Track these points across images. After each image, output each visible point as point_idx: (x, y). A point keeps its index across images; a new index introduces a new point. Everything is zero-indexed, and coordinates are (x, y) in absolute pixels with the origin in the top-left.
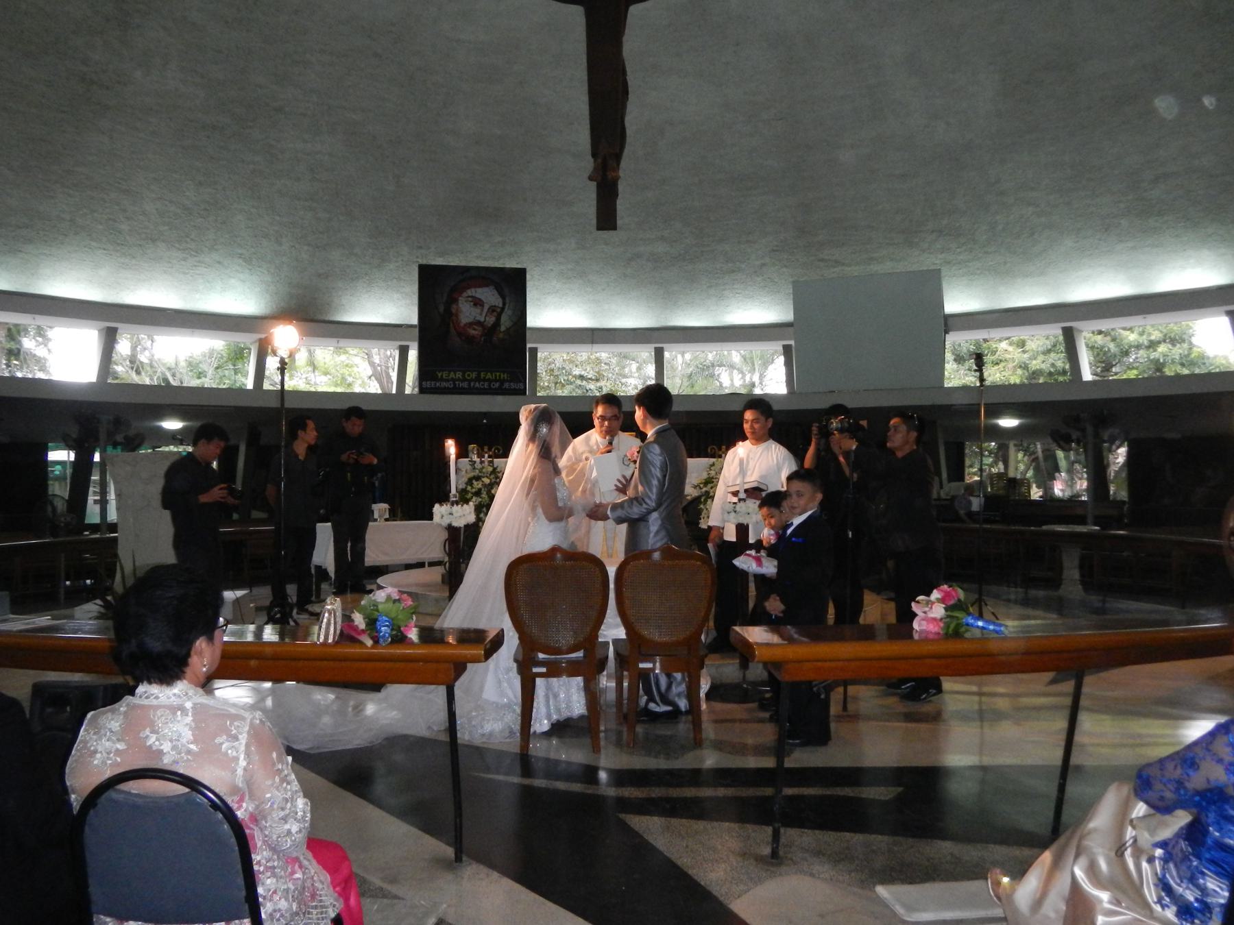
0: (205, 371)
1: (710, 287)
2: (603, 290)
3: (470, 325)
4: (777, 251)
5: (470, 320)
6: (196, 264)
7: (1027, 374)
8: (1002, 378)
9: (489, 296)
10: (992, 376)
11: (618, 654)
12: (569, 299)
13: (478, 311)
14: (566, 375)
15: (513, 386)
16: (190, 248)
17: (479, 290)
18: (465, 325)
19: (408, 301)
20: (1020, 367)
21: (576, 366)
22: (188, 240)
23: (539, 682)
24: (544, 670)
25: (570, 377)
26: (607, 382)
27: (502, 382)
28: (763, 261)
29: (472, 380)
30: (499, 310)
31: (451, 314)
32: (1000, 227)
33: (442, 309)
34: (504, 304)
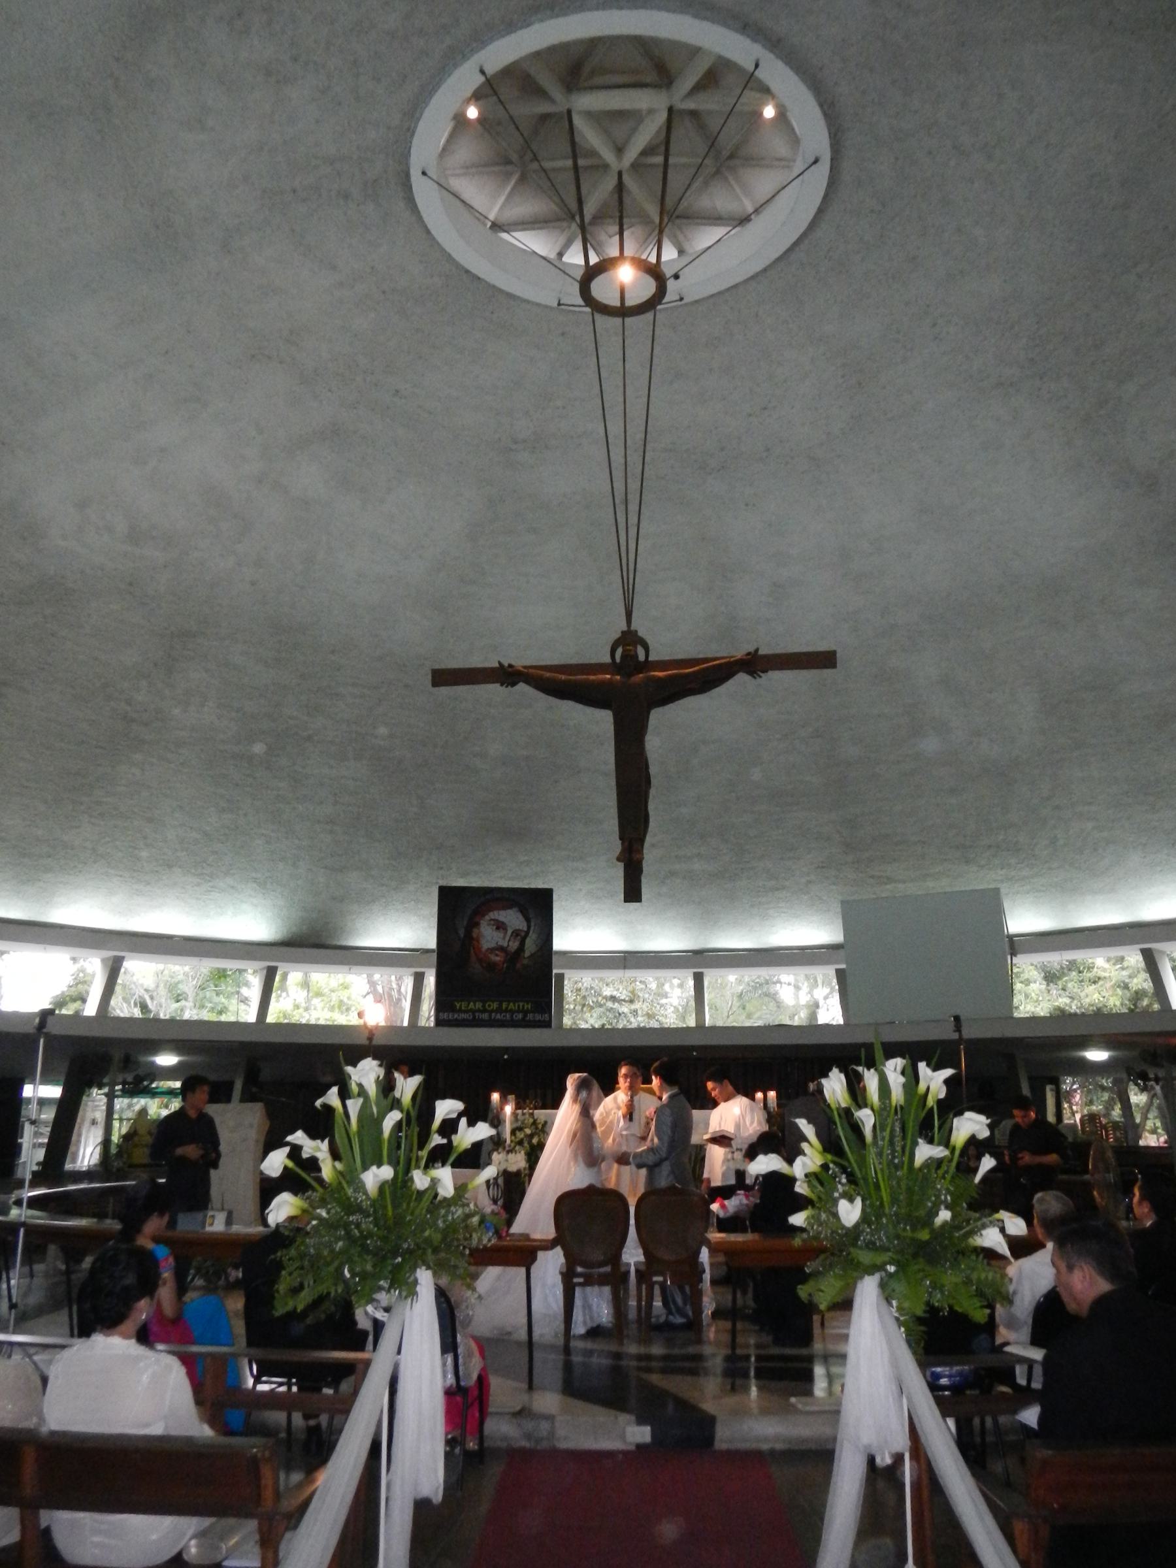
0: (185, 993)
1: (752, 906)
2: (636, 910)
3: (492, 950)
4: (823, 867)
5: (493, 945)
6: (209, 889)
7: (1128, 995)
8: (1101, 999)
9: (513, 918)
10: (1089, 997)
11: (637, 1271)
13: (501, 935)
14: (595, 996)
15: (538, 1017)
17: (502, 913)
19: (426, 924)
20: (1119, 986)
21: (607, 985)
23: (578, 1291)
24: (581, 1280)
25: (600, 998)
26: (643, 1004)
27: (525, 1013)
28: (808, 878)
29: (492, 1011)
30: (523, 934)
31: (472, 938)
32: (1061, 842)
33: (462, 932)
34: (529, 927)
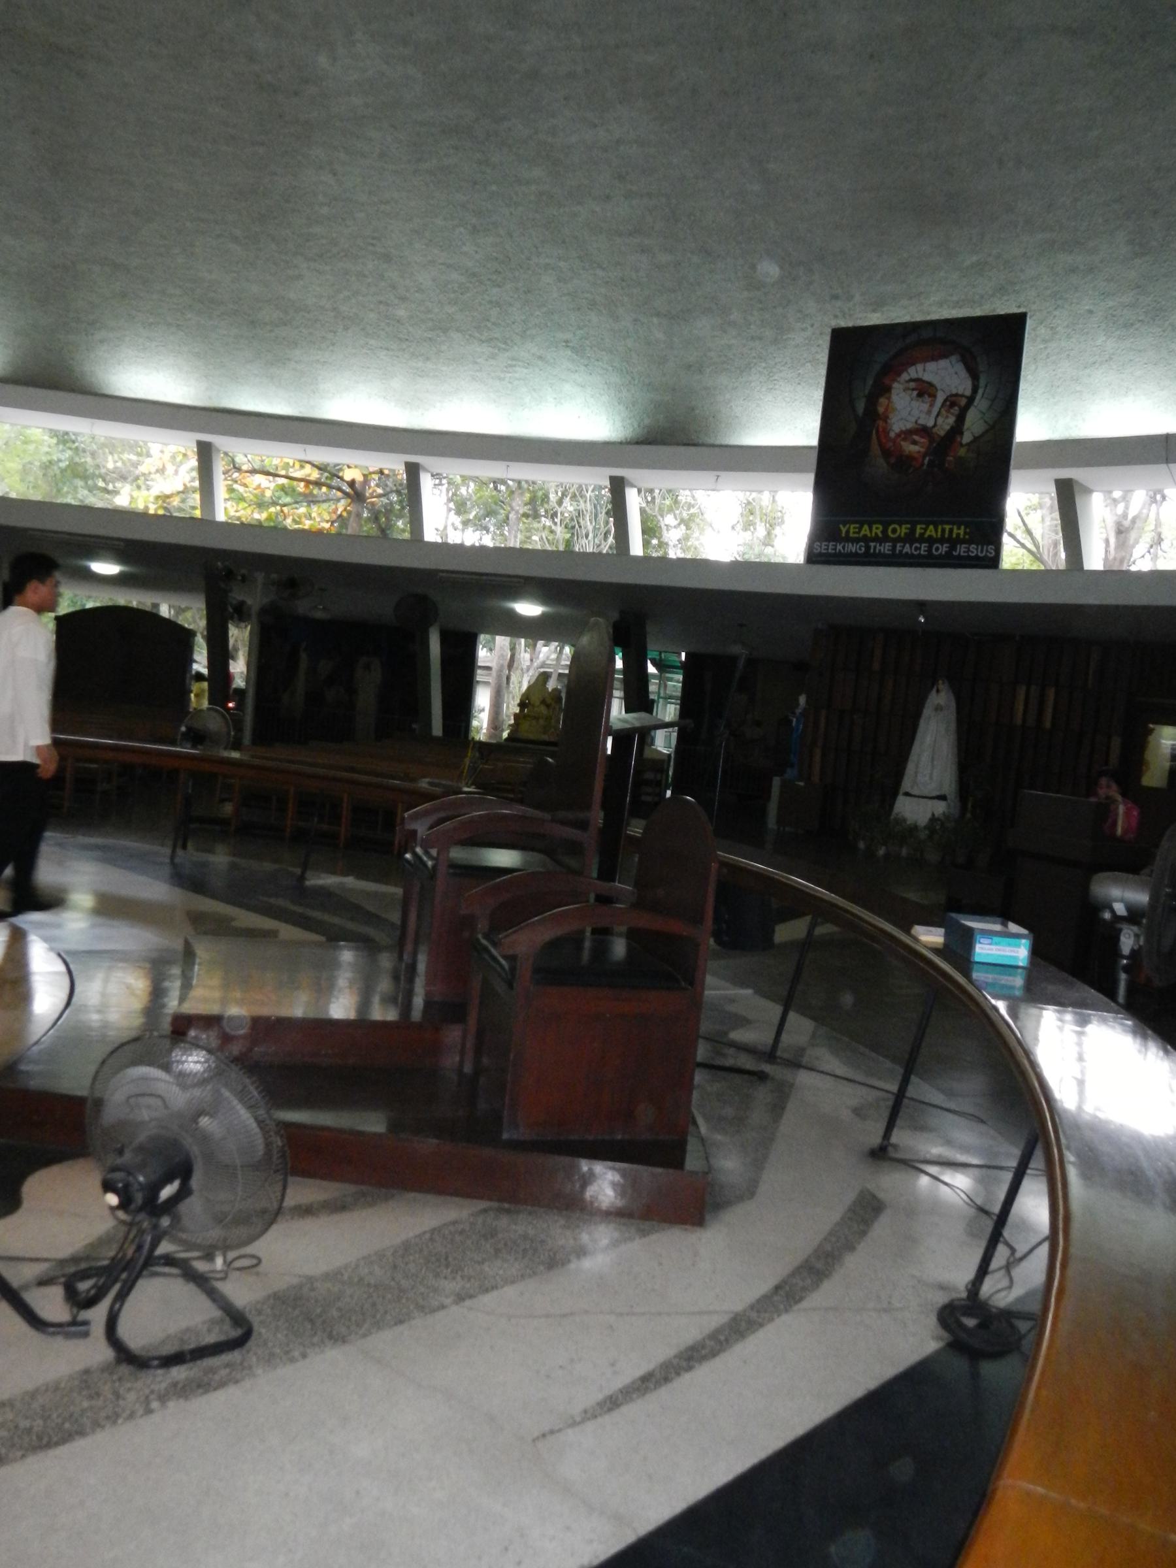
3: (907, 434)
12: (1138, 373)
13: (925, 407)
15: (974, 550)
16: (496, 338)
17: (931, 366)
18: (898, 435)
22: (489, 324)
27: (954, 542)
29: (899, 539)
30: (963, 402)
33: (860, 407)
34: (975, 390)
